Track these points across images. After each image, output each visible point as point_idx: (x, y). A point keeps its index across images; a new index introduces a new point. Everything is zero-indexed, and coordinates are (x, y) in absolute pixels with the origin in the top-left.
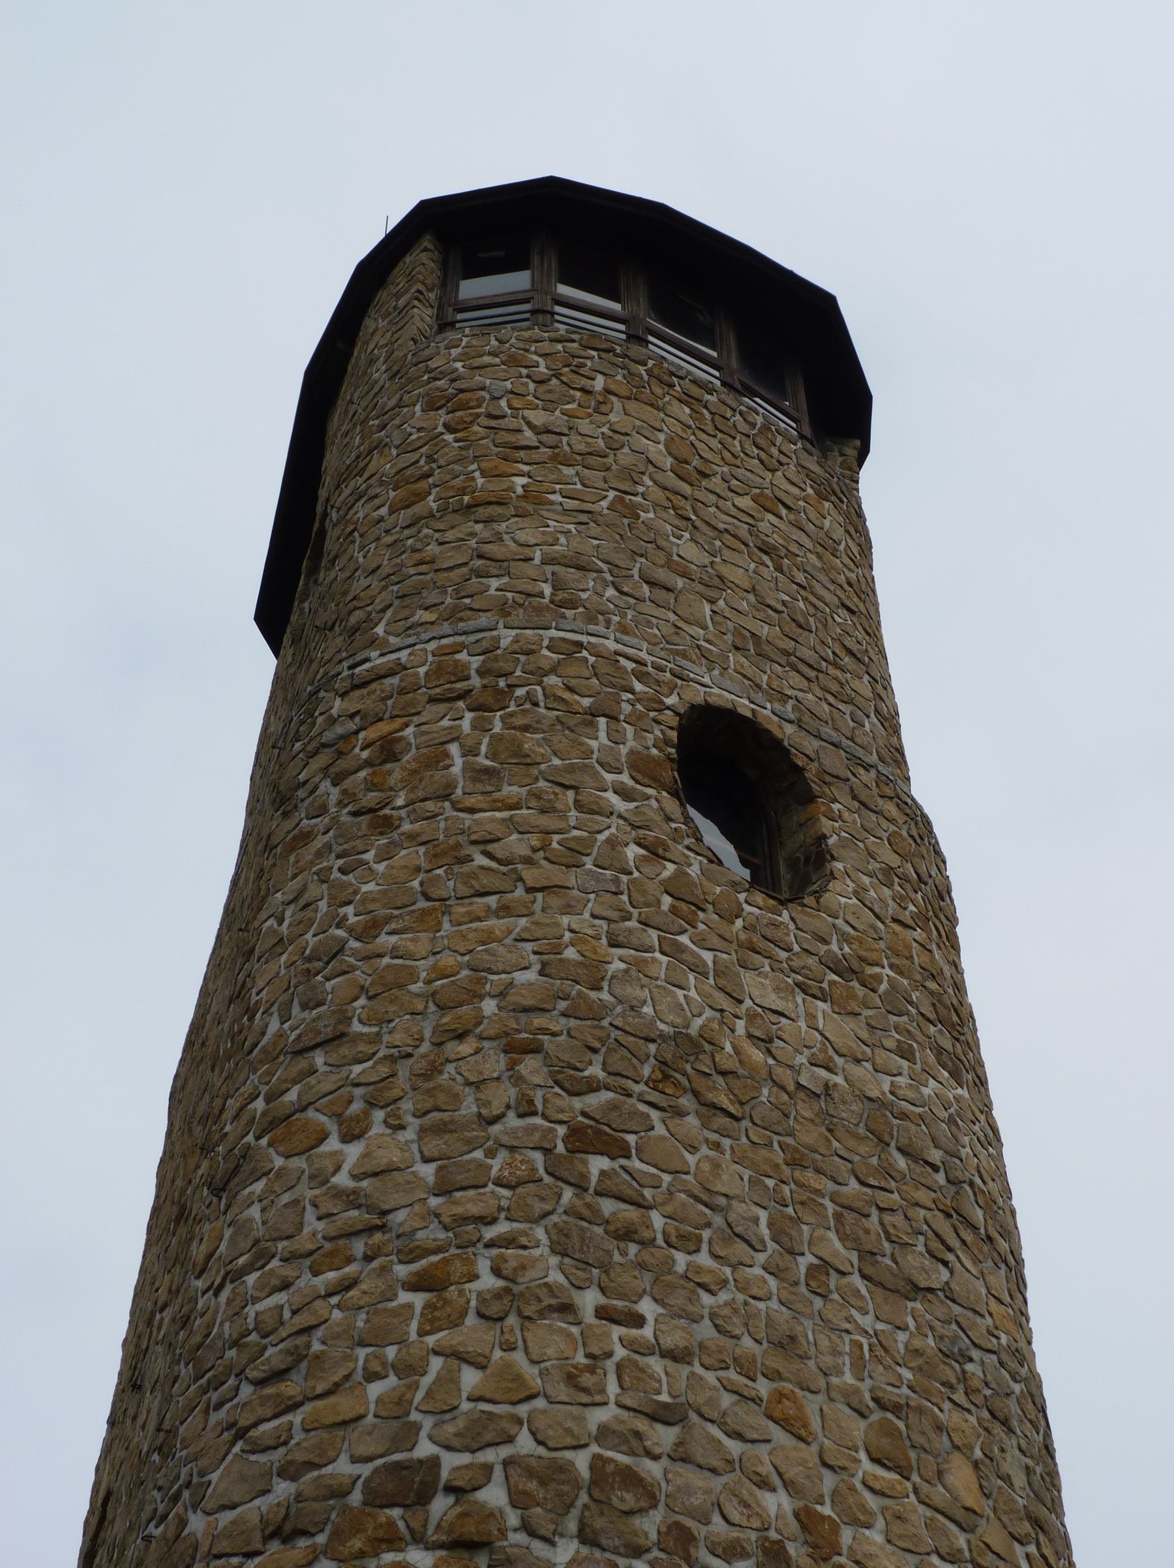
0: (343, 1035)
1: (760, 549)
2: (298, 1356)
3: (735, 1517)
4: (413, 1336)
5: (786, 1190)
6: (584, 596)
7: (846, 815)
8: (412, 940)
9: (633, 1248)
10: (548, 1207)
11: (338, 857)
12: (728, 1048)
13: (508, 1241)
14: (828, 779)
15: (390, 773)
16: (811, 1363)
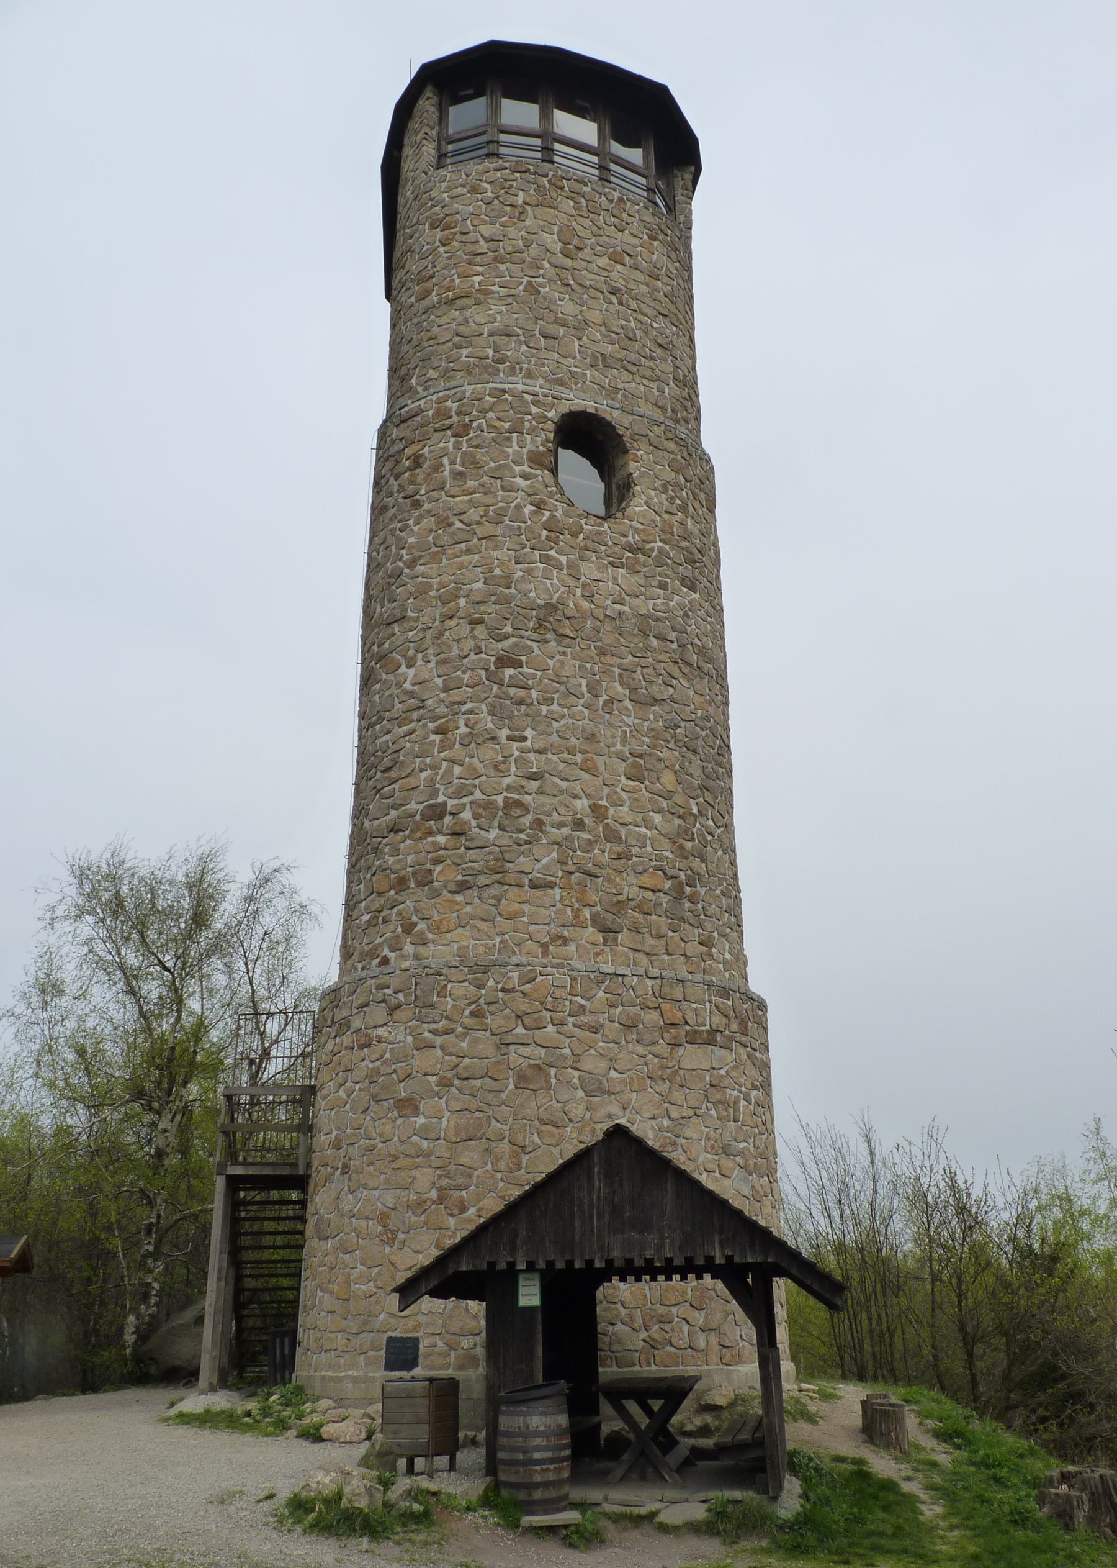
0: (404, 617)
1: (610, 293)
2: (395, 762)
3: (562, 812)
4: (436, 754)
5: (596, 667)
6: (509, 354)
7: (645, 457)
8: (430, 568)
9: (523, 708)
10: (487, 695)
11: (399, 522)
12: (571, 605)
13: (471, 712)
14: (636, 437)
15: (418, 475)
16: (602, 744)
